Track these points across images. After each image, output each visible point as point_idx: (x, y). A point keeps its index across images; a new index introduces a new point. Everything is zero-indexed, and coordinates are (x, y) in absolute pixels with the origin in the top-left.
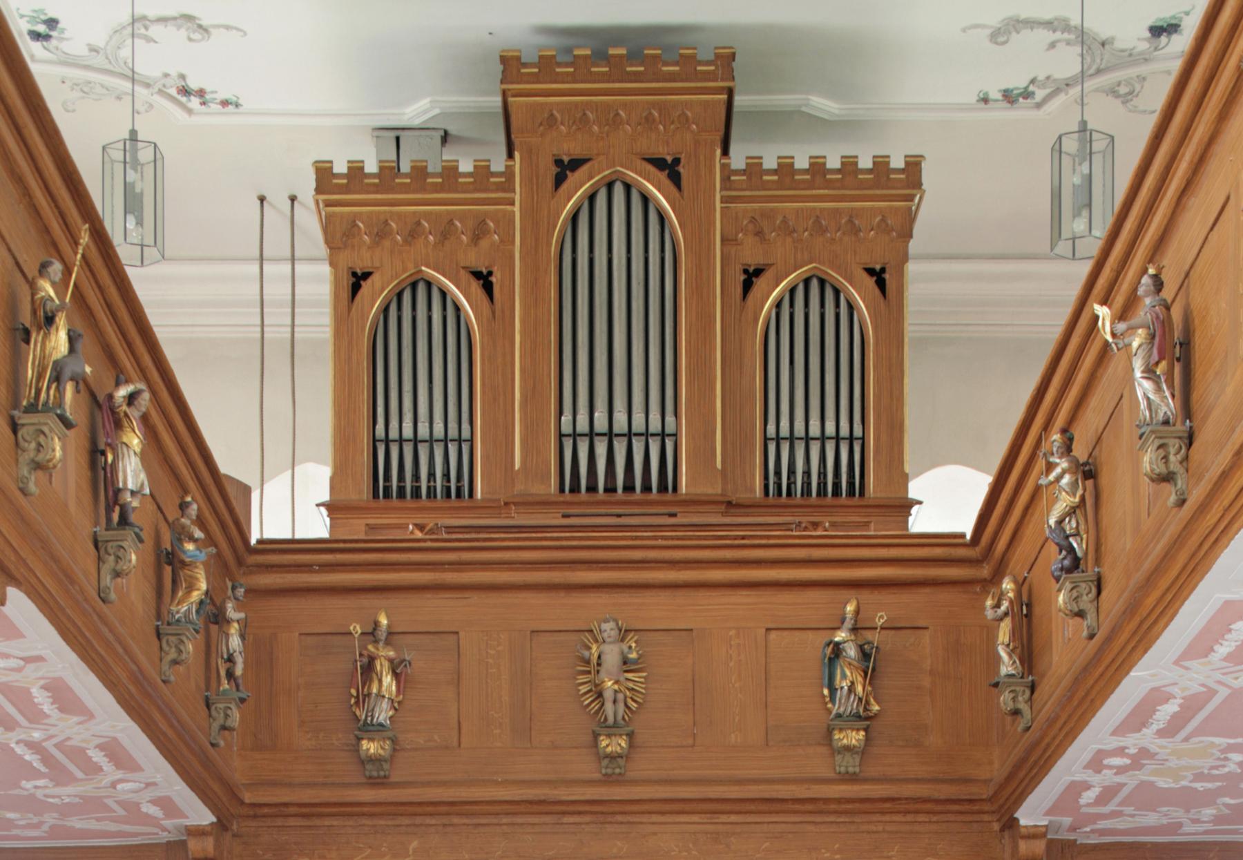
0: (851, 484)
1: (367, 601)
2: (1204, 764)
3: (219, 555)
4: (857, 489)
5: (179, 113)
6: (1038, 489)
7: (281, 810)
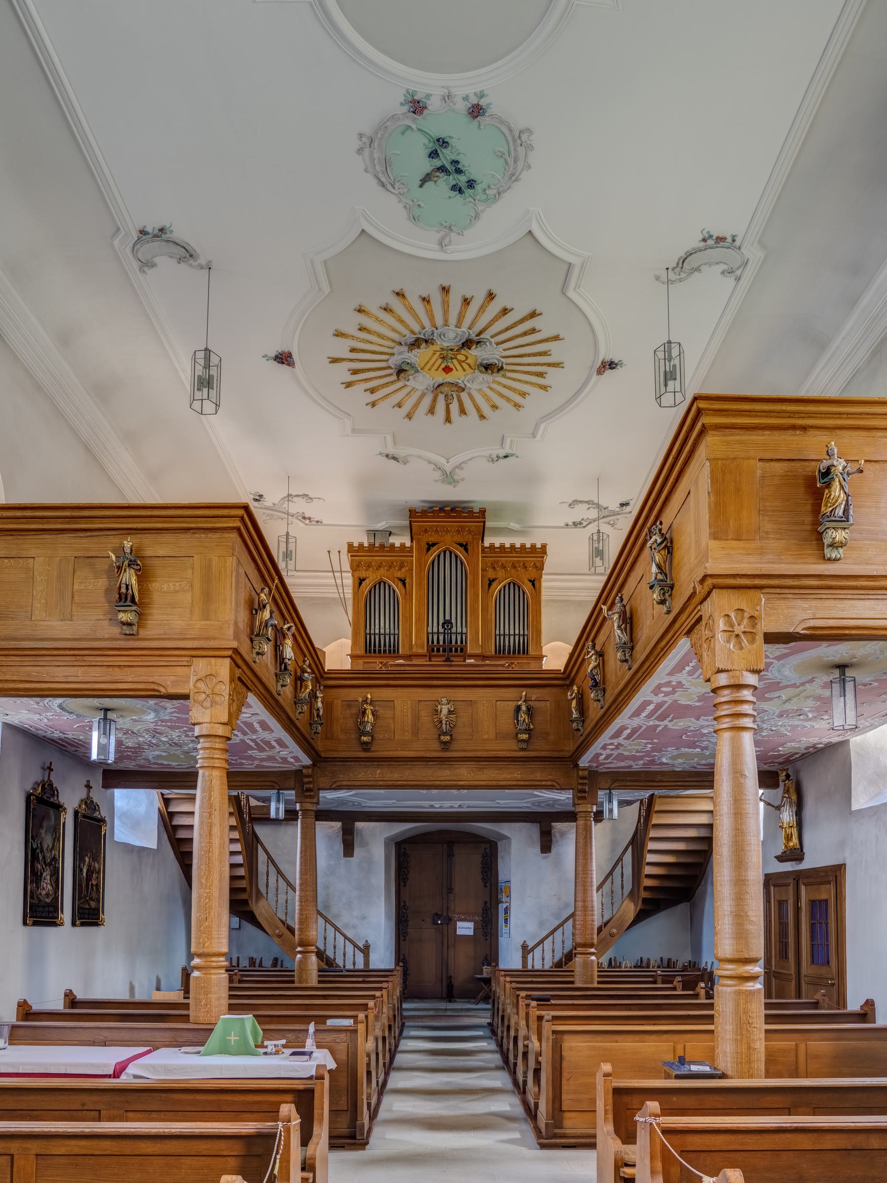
0: (524, 650)
1: (363, 690)
2: (639, 748)
3: (316, 677)
4: (525, 652)
5: (302, 525)
6: (584, 660)
7: (334, 759)
